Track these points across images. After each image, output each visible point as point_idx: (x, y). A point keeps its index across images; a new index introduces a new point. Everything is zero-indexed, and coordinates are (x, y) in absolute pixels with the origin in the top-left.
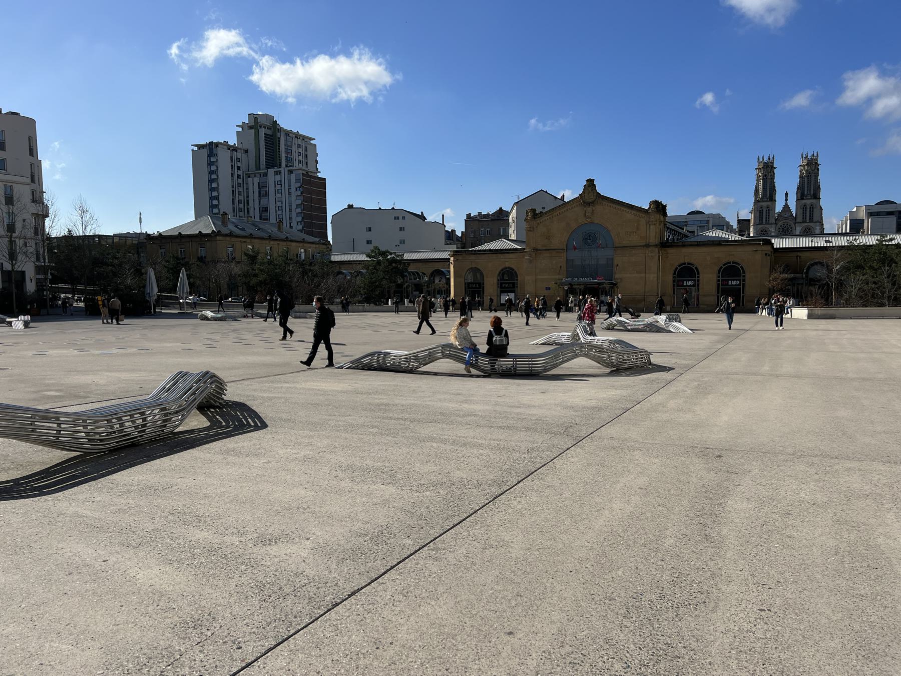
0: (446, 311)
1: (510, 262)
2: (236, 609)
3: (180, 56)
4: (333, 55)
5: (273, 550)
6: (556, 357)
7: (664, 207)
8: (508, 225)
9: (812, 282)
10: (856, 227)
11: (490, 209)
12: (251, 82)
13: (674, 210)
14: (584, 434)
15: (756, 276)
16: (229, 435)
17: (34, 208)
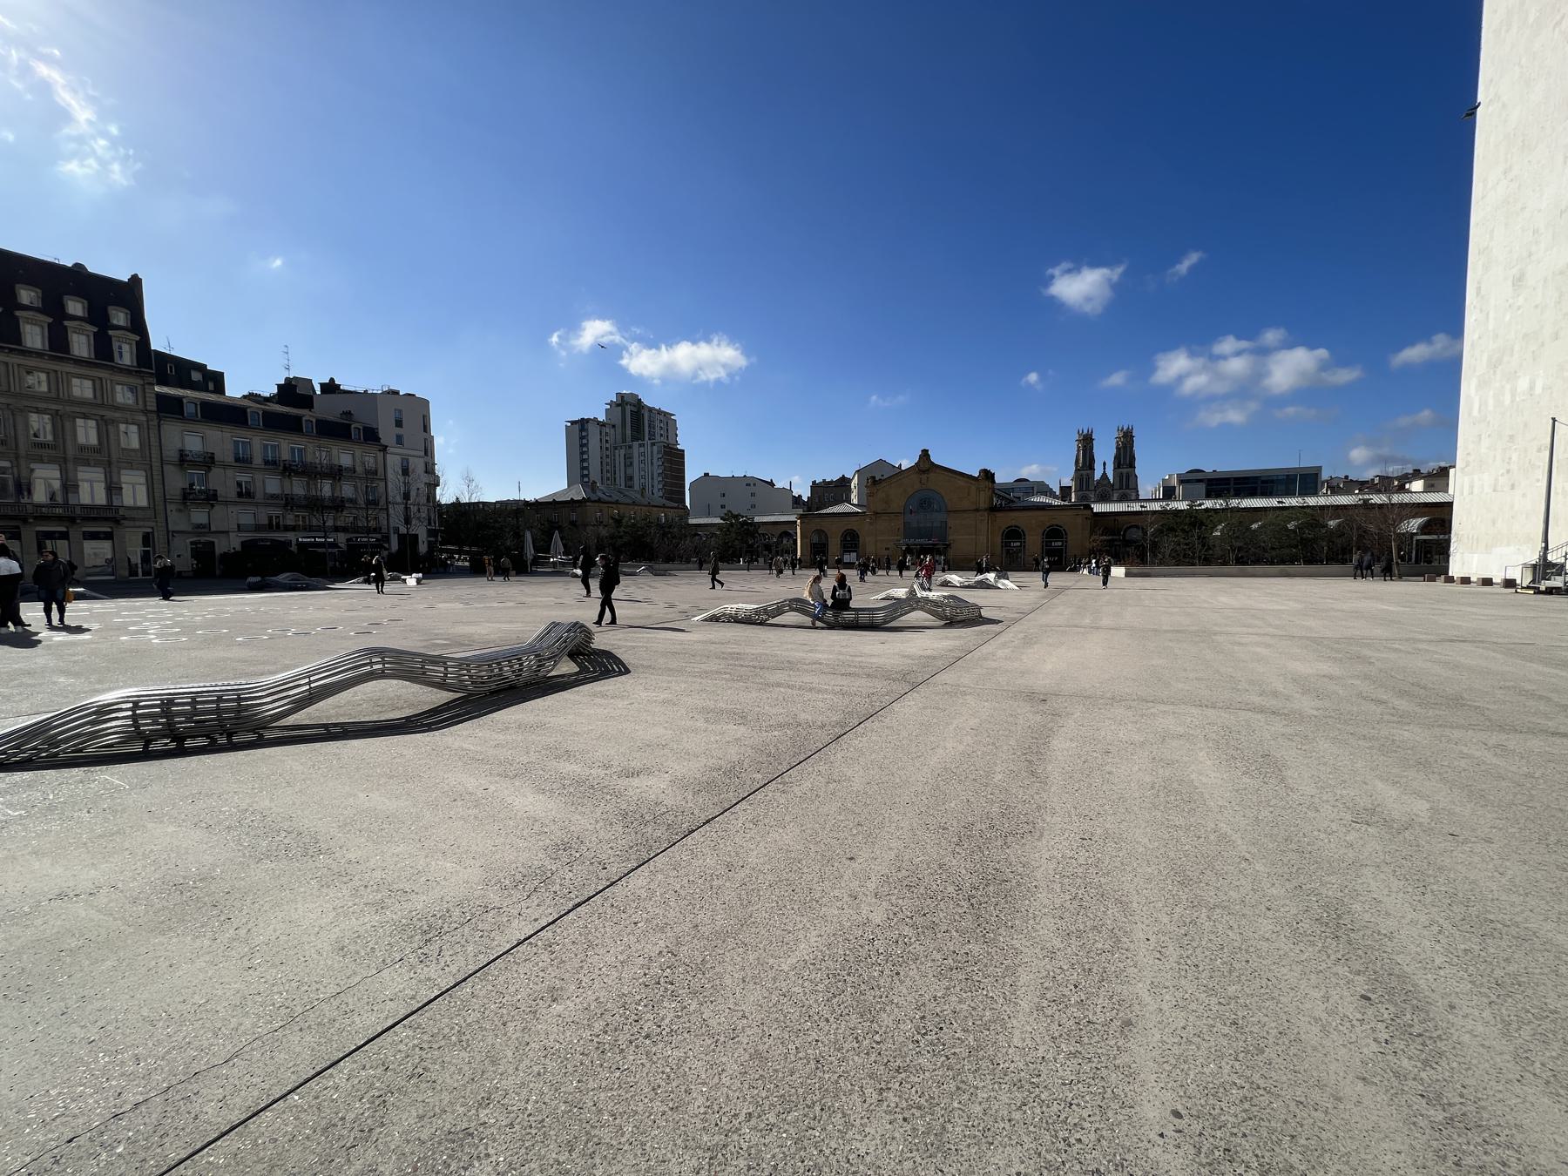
0: (794, 568)
1: (853, 524)
2: (602, 834)
3: (559, 344)
4: (694, 342)
5: (635, 782)
6: (895, 611)
7: (993, 475)
8: (850, 491)
9: (1128, 543)
10: (1169, 493)
11: (833, 476)
12: (621, 366)
13: (1001, 478)
14: (920, 679)
15: (1077, 537)
16: (596, 679)
17: (426, 478)
